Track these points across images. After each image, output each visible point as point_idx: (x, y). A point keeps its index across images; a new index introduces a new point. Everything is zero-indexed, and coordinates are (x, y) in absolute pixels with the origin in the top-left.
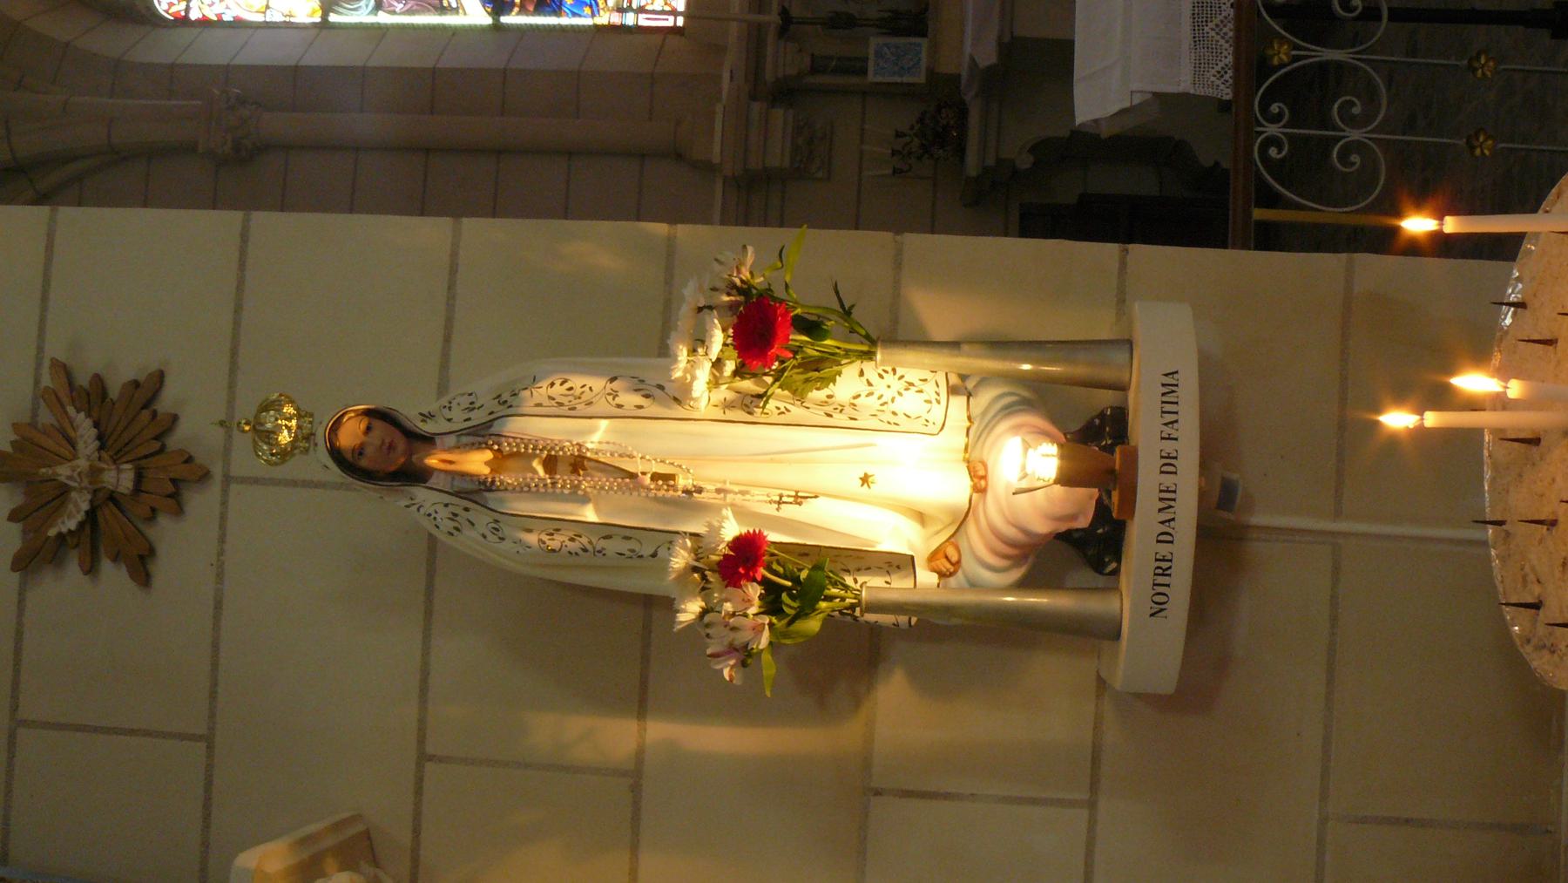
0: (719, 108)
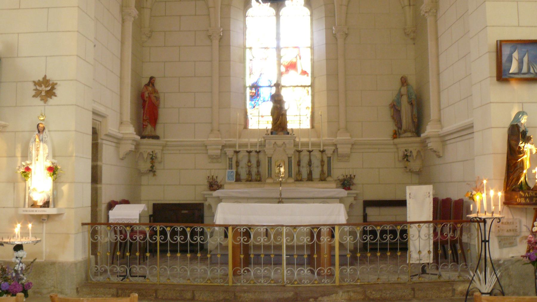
0: (220, 139)
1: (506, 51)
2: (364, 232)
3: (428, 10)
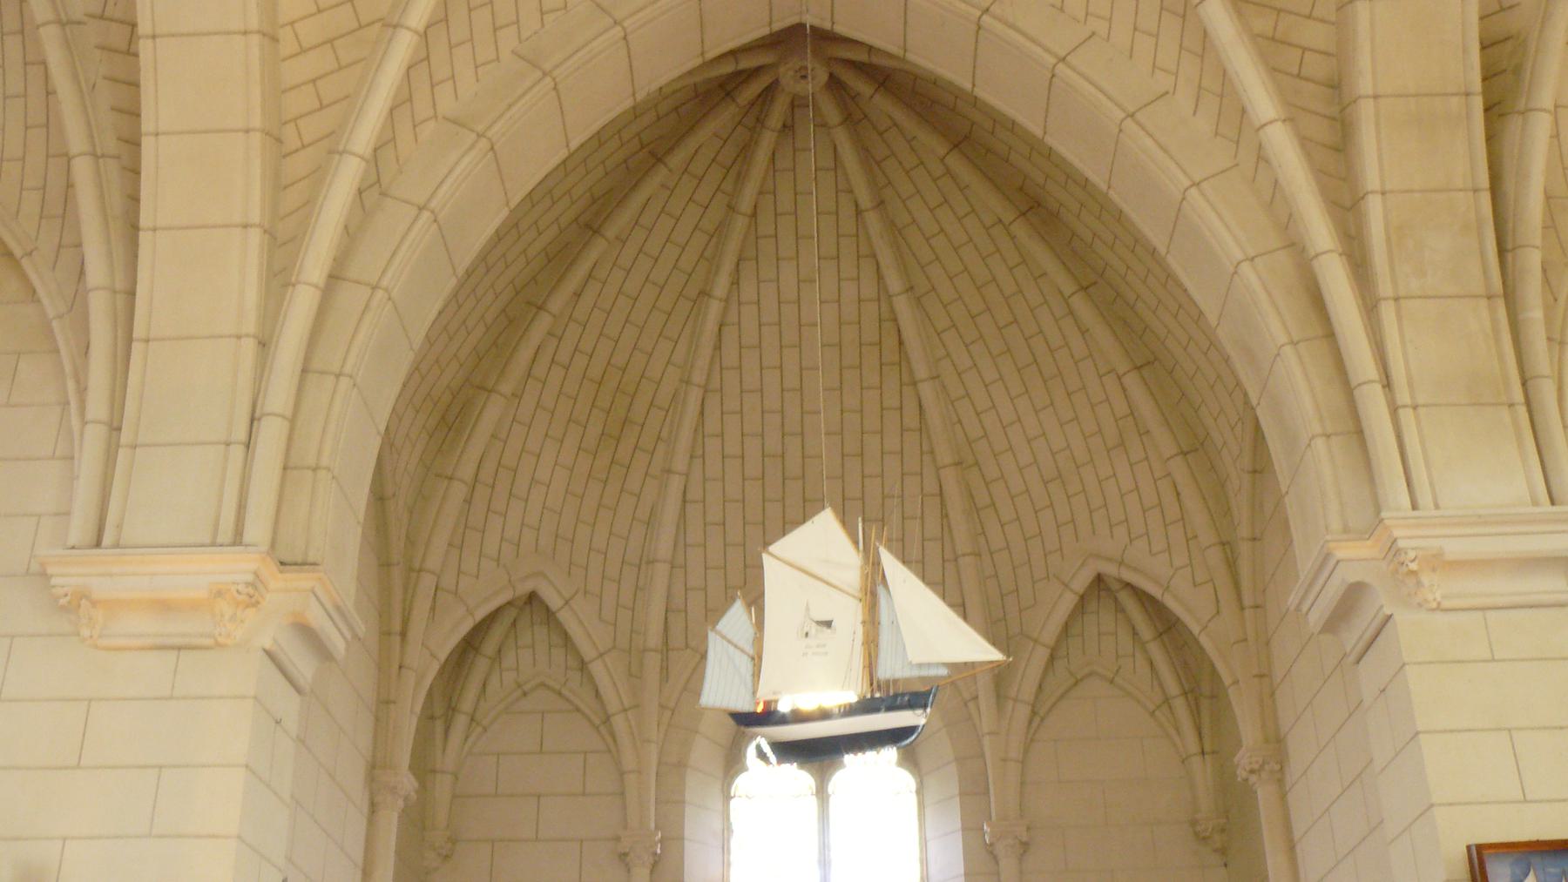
3: (1256, 767)
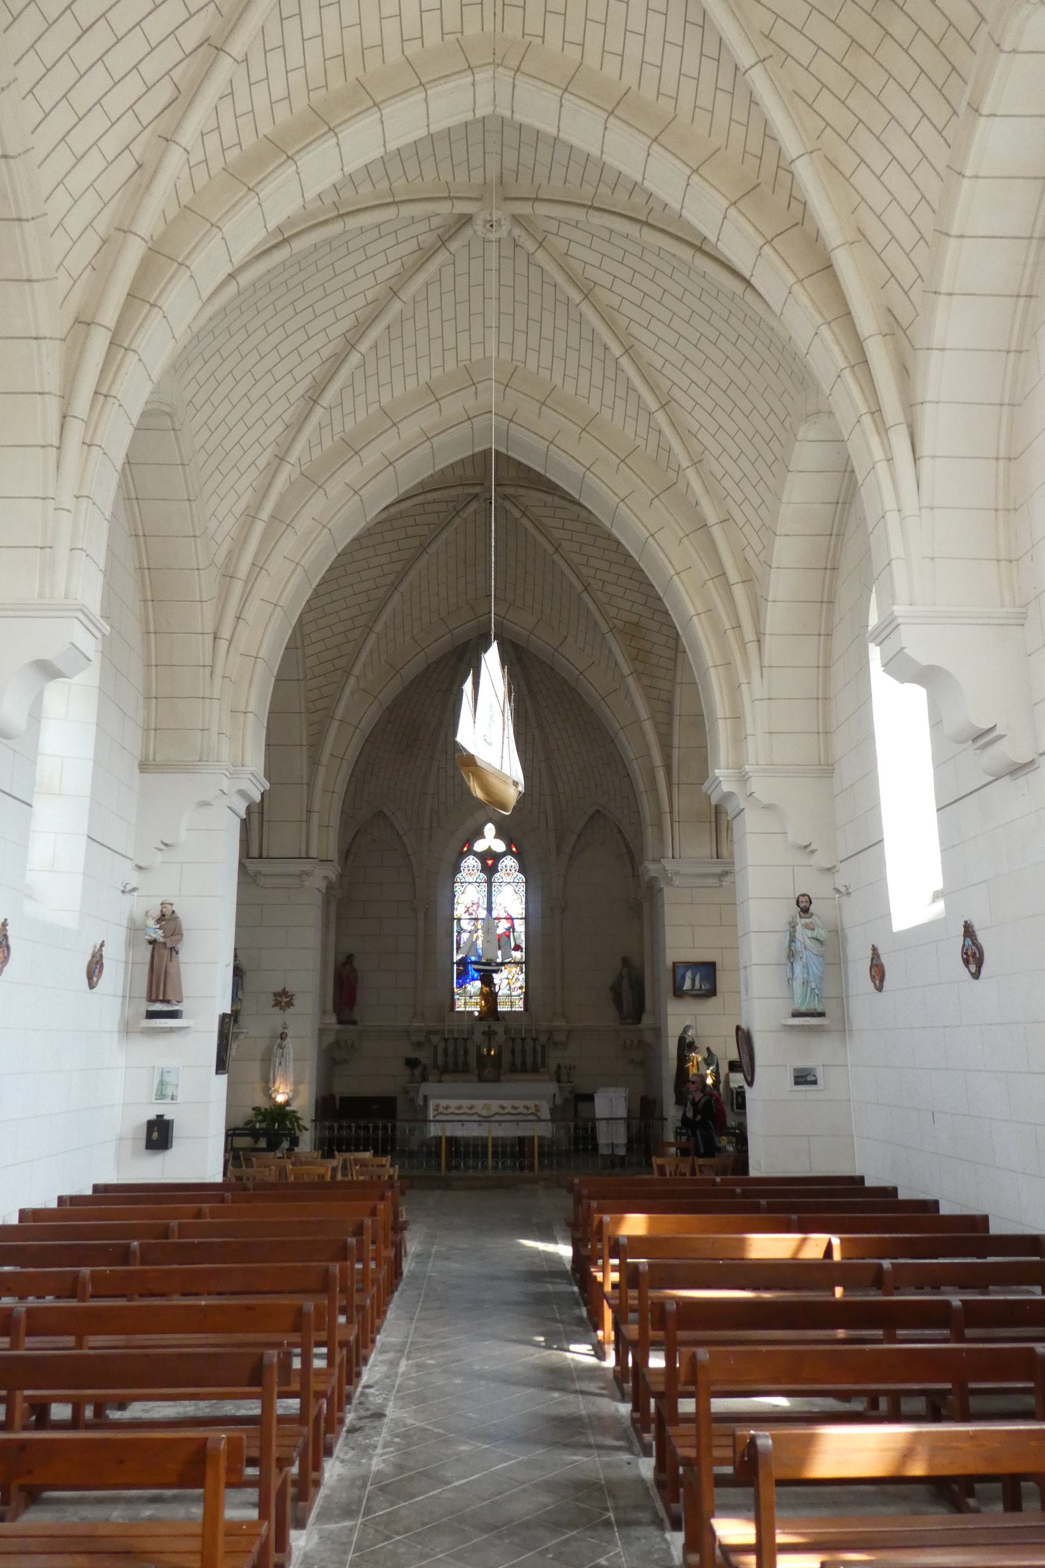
1: (680, 971)
2: (576, 1127)
